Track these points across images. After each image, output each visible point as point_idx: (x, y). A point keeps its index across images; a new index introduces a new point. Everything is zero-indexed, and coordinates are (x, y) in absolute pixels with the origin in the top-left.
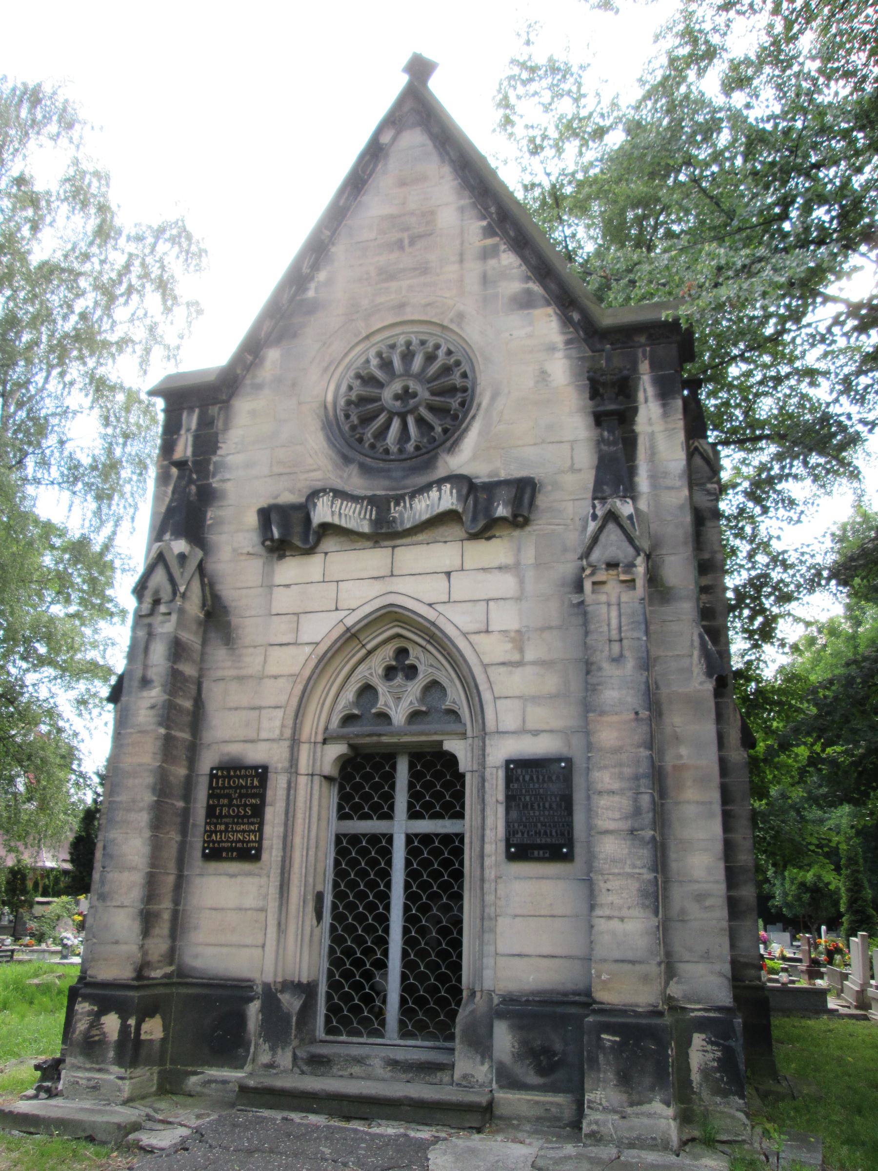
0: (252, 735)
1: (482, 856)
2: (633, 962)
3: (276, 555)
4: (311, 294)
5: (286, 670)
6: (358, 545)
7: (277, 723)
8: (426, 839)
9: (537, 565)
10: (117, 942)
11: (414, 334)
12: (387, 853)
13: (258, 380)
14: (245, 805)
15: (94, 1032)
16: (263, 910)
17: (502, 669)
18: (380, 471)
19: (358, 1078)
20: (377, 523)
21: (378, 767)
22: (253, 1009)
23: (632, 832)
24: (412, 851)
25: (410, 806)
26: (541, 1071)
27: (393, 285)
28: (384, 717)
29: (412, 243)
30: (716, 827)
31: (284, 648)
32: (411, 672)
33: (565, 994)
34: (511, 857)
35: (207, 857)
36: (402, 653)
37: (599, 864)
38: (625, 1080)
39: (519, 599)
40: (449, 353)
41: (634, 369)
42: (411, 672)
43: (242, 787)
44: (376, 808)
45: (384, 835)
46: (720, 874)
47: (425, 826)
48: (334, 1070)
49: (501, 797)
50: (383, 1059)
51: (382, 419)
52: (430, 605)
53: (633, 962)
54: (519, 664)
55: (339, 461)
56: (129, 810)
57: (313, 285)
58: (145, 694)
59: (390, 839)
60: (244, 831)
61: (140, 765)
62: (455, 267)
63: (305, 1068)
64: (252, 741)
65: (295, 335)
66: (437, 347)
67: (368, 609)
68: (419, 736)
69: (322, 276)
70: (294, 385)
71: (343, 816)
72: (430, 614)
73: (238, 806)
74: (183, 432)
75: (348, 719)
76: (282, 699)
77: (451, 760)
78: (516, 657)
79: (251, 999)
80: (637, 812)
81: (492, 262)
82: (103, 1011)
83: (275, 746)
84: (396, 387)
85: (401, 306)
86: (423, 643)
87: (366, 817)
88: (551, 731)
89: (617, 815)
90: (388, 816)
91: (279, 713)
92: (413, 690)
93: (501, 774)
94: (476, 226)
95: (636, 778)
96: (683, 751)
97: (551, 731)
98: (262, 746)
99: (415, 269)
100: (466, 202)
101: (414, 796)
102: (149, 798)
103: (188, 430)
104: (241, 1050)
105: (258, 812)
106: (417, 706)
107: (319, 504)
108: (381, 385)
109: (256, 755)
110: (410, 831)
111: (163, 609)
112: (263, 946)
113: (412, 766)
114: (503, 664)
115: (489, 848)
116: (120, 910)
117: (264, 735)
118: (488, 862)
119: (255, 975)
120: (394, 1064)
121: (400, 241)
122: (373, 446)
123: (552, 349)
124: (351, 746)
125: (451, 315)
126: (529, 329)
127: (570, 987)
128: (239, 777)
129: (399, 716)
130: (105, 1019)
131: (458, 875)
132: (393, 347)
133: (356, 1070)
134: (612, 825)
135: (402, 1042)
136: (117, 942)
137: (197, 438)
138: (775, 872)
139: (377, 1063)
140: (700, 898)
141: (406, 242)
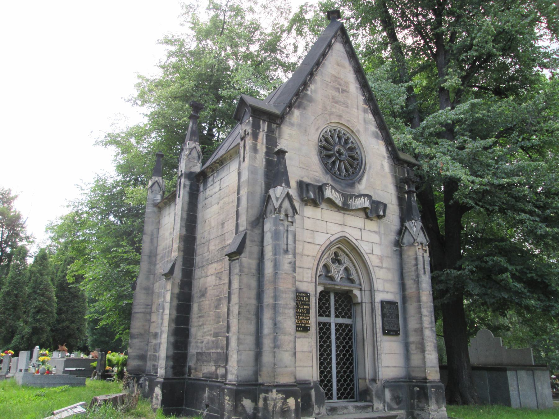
0: (302, 280)
2: (434, 367)
3: (304, 203)
4: (309, 93)
6: (333, 209)
7: (310, 275)
9: (384, 234)
10: (286, 367)
11: (343, 130)
14: (304, 309)
15: (285, 407)
16: (311, 352)
17: (377, 268)
18: (338, 181)
19: (345, 414)
22: (313, 392)
23: (431, 328)
26: (398, 404)
28: (332, 278)
31: (310, 244)
32: (339, 262)
33: (399, 379)
34: (384, 333)
36: (336, 254)
37: (425, 338)
38: (437, 402)
39: (380, 244)
40: (352, 143)
42: (339, 262)
43: (302, 301)
45: (328, 323)
47: (340, 320)
48: (338, 412)
50: (353, 406)
51: (334, 159)
52: (356, 240)
53: (434, 367)
54: (382, 268)
55: (324, 172)
56: (285, 308)
58: (286, 256)
59: (330, 325)
60: (304, 319)
61: (288, 288)
63: (329, 413)
64: (301, 282)
65: (304, 108)
66: (348, 138)
68: (345, 286)
70: (306, 130)
73: (301, 309)
74: (261, 130)
76: (311, 266)
78: (380, 265)
79: (312, 388)
81: (367, 115)
82: (287, 397)
83: (310, 285)
84: (337, 148)
86: (348, 253)
88: (391, 292)
89: (428, 323)
90: (328, 316)
91: (310, 271)
93: (379, 305)
94: (361, 98)
97: (391, 292)
98: (306, 284)
100: (358, 86)
103: (263, 131)
104: (310, 409)
107: (327, 189)
110: (337, 322)
112: (312, 367)
113: (335, 297)
114: (377, 267)
116: (286, 353)
117: (305, 280)
118: (378, 335)
120: (357, 407)
121: (338, 88)
124: (325, 288)
126: (378, 147)
127: (400, 376)
128: (301, 296)
130: (288, 400)
133: (345, 411)
134: (427, 326)
135: (338, 401)
136: (286, 367)
137: (267, 136)
139: (350, 407)
141: (341, 90)
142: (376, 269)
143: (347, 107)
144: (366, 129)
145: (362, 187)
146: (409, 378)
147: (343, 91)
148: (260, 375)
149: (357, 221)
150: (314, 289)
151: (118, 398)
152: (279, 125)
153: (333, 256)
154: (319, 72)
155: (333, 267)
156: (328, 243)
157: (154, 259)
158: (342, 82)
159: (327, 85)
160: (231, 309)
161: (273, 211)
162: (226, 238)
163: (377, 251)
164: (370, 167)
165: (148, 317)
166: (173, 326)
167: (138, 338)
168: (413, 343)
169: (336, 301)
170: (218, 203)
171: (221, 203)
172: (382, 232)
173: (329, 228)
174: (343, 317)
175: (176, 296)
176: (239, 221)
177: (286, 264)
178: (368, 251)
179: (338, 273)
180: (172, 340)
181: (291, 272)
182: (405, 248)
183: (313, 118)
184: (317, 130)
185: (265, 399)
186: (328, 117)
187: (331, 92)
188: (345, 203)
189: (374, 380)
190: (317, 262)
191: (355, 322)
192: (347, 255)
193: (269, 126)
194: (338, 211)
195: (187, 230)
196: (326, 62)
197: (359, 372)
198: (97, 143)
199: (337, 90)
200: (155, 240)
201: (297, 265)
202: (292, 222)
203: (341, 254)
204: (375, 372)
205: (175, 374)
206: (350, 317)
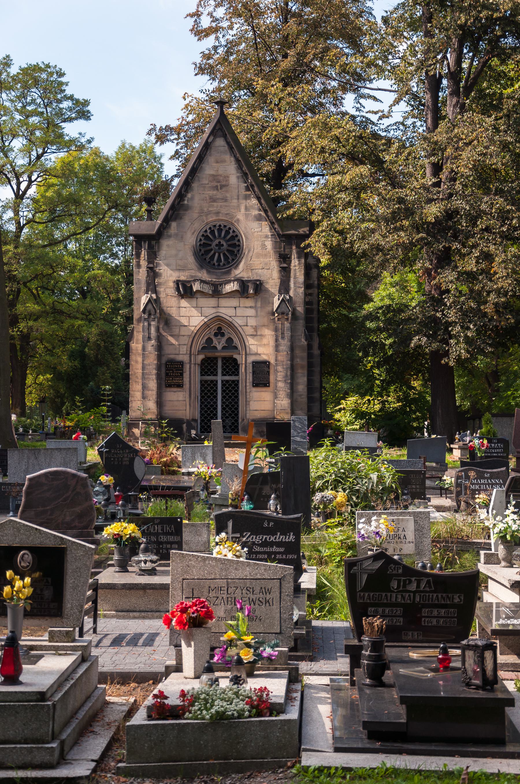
1: (246, 386)
4: (186, 202)
5: (186, 334)
7: (185, 349)
8: (227, 381)
9: (261, 307)
12: (216, 385)
13: (169, 234)
16: (185, 401)
18: (213, 272)
20: (214, 291)
21: (212, 361)
24: (223, 385)
25: (222, 372)
27: (215, 204)
28: (215, 348)
29: (221, 188)
30: (305, 379)
32: (223, 335)
35: (166, 387)
41: (291, 252)
42: (223, 335)
44: (212, 373)
46: (306, 390)
47: (227, 378)
49: (251, 371)
51: (212, 252)
57: (186, 199)
59: (217, 381)
62: (236, 201)
65: (181, 218)
66: (230, 228)
67: (211, 317)
69: (189, 195)
70: (182, 237)
71: (202, 375)
72: (230, 320)
75: (203, 348)
76: (186, 342)
77: (235, 360)
78: (255, 333)
80: (286, 376)
84: (217, 242)
85: (218, 213)
87: (209, 375)
90: (216, 375)
91: (185, 346)
92: (224, 340)
93: (251, 365)
95: (287, 368)
96: (298, 360)
99: (223, 199)
101: (223, 370)
102: (155, 372)
105: (182, 374)
106: (225, 345)
108: (211, 240)
109: (180, 358)
111: (152, 317)
113: (222, 361)
115: (248, 384)
117: (181, 353)
119: (184, 418)
121: (217, 186)
122: (209, 262)
123: (267, 237)
125: (235, 219)
129: (219, 347)
131: (237, 391)
132: (215, 226)
138: (471, 307)
140: (301, 395)
147: (222, 187)
150: (188, 358)
151: (494, 606)
154: (197, 178)
179: (219, 344)
183: (190, 223)
184: (193, 233)
186: (204, 218)
190: (191, 339)
196: (203, 165)
198: (196, 75)
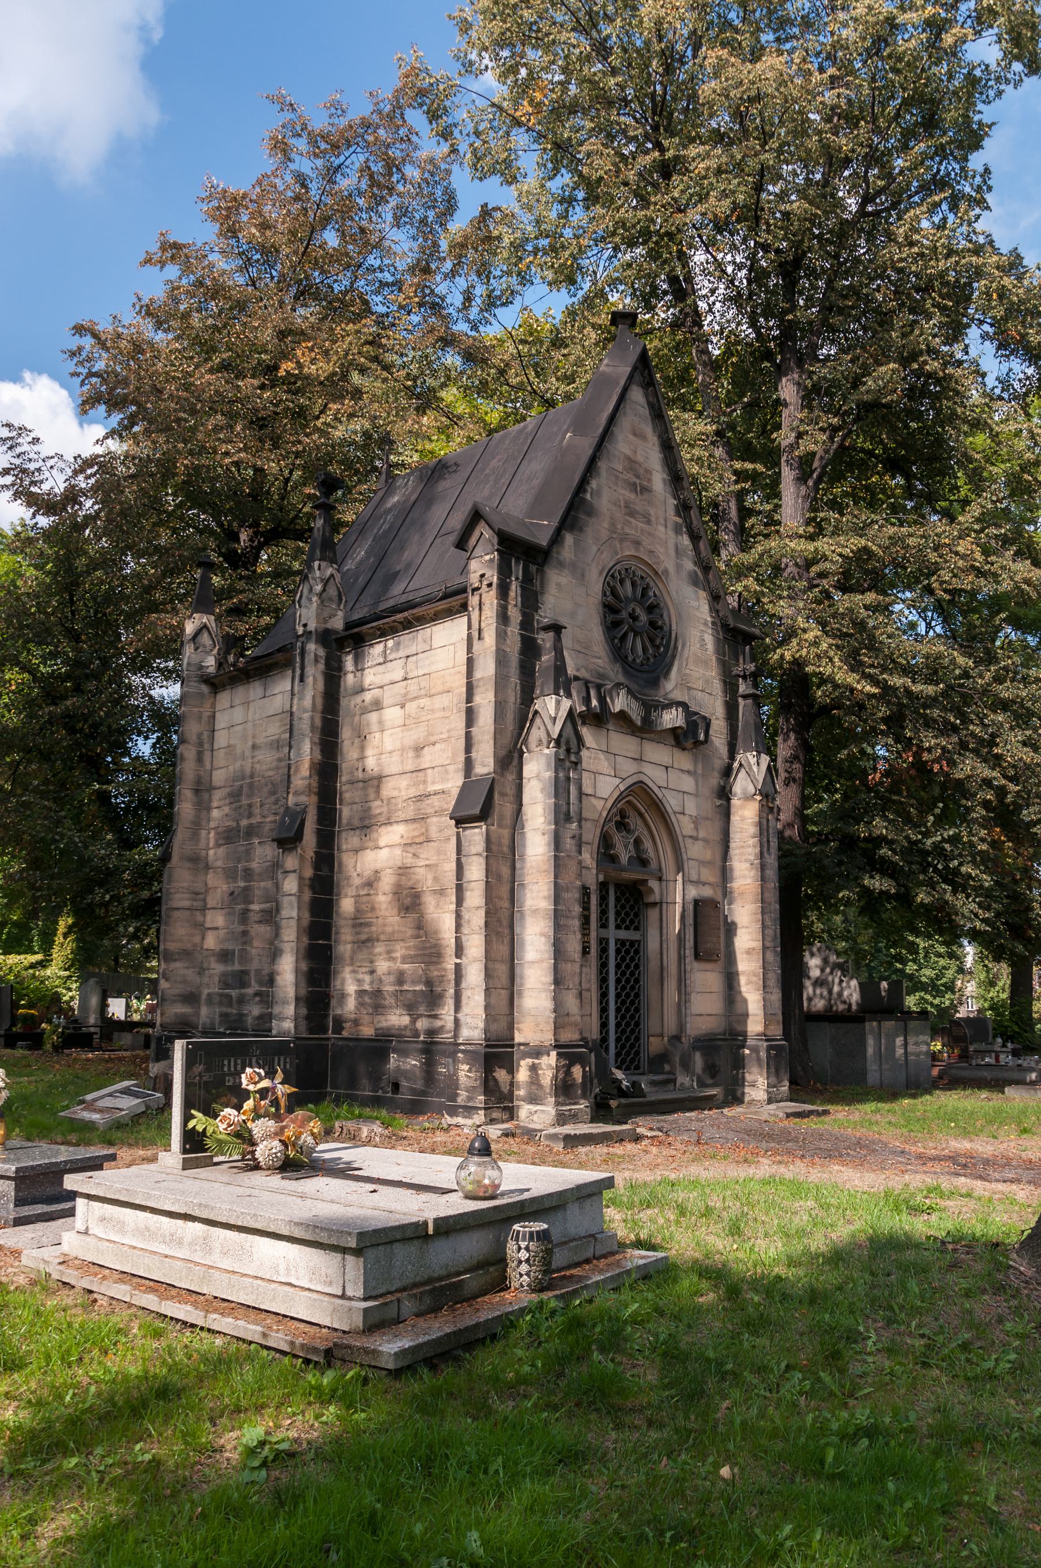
11: (640, 570)
26: (713, 1077)
39: (696, 795)
47: (623, 934)
70: (583, 575)
121: (635, 484)
142: (689, 841)
143: (649, 522)
144: (679, 567)
145: (671, 687)
146: (731, 1034)
148: (519, 1030)
149: (659, 753)
152: (541, 571)
153: (618, 818)
155: (617, 838)
156: (615, 796)
157: (206, 796)
158: (641, 471)
159: (617, 477)
160: (466, 915)
161: (545, 742)
162: (429, 779)
163: (691, 807)
164: (684, 645)
165: (199, 918)
166: (305, 940)
167: (180, 960)
168: (744, 973)
169: (617, 900)
170: (403, 706)
171: (411, 707)
172: (700, 771)
173: (618, 766)
174: (627, 928)
175: (307, 882)
176: (473, 755)
177: (569, 840)
178: (677, 809)
180: (304, 966)
181: (574, 854)
182: (735, 802)
185: (534, 1068)
187: (623, 492)
188: (647, 720)
189: (676, 1038)
191: (644, 936)
192: (641, 815)
193: (526, 570)
194: (633, 734)
195: (322, 752)
197: (652, 1024)
199: (633, 487)
200: (207, 755)
201: (584, 839)
202: (576, 764)
203: (631, 813)
204: (681, 1026)
205: (311, 1030)
206: (637, 929)
